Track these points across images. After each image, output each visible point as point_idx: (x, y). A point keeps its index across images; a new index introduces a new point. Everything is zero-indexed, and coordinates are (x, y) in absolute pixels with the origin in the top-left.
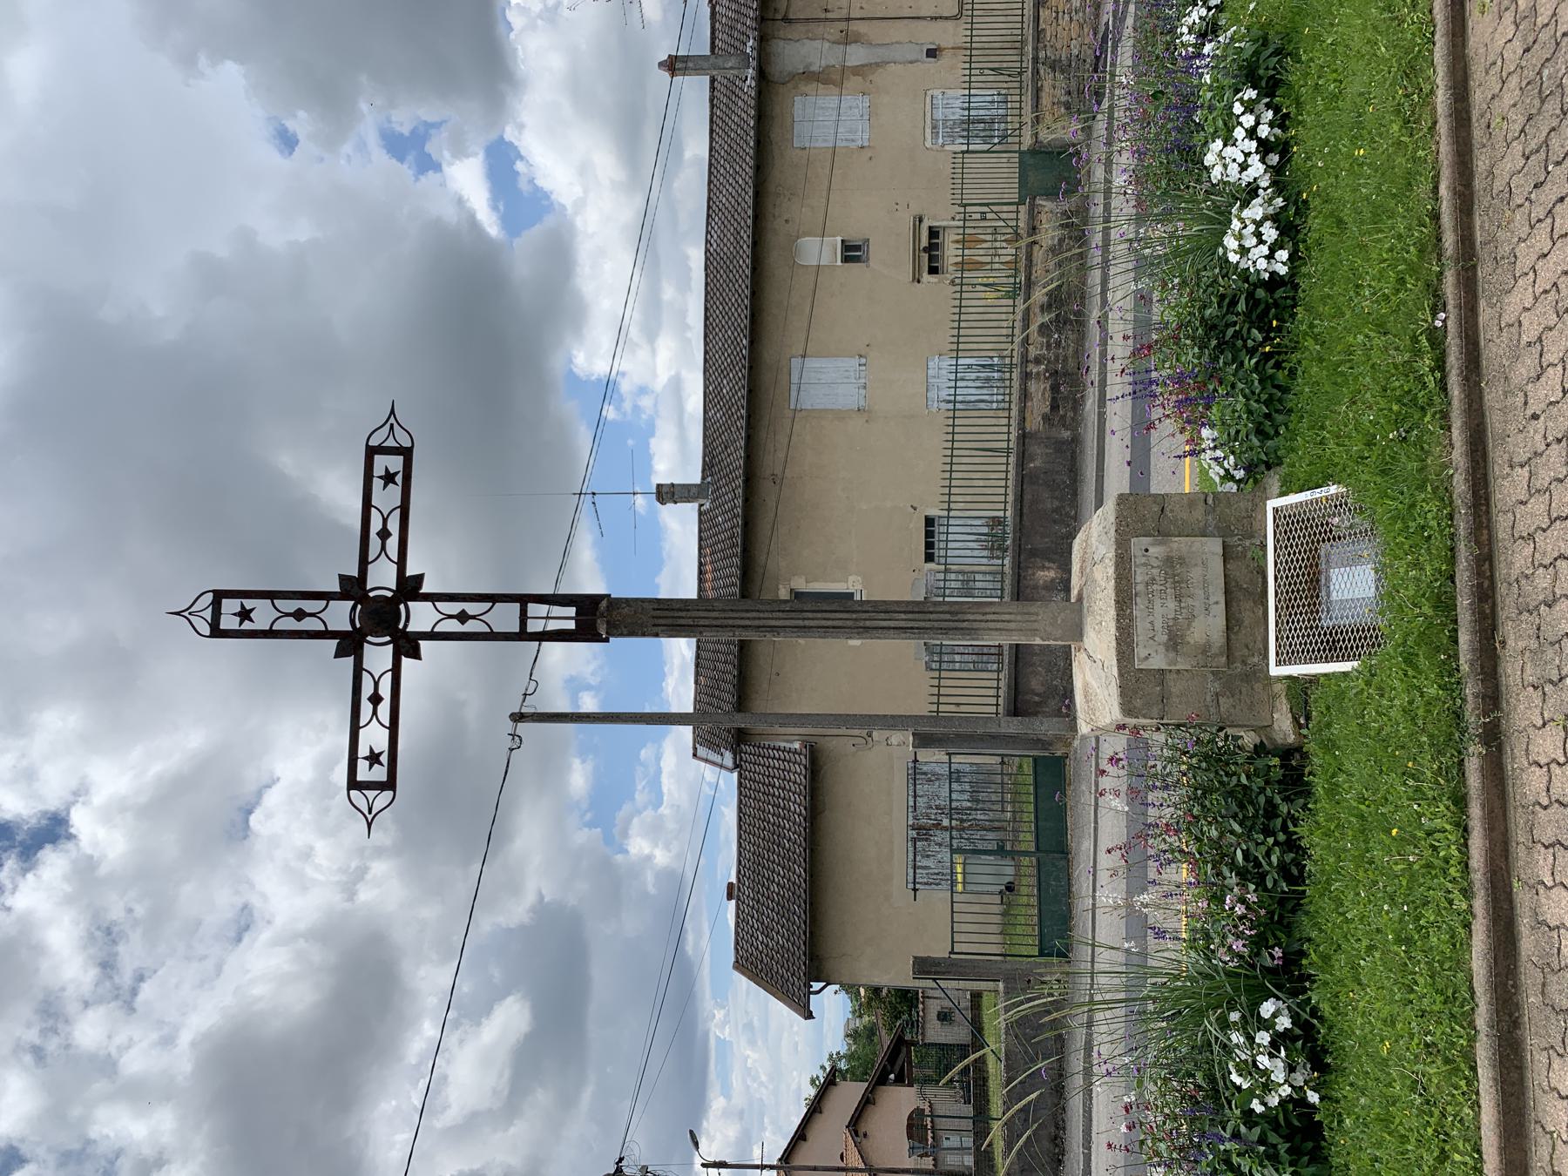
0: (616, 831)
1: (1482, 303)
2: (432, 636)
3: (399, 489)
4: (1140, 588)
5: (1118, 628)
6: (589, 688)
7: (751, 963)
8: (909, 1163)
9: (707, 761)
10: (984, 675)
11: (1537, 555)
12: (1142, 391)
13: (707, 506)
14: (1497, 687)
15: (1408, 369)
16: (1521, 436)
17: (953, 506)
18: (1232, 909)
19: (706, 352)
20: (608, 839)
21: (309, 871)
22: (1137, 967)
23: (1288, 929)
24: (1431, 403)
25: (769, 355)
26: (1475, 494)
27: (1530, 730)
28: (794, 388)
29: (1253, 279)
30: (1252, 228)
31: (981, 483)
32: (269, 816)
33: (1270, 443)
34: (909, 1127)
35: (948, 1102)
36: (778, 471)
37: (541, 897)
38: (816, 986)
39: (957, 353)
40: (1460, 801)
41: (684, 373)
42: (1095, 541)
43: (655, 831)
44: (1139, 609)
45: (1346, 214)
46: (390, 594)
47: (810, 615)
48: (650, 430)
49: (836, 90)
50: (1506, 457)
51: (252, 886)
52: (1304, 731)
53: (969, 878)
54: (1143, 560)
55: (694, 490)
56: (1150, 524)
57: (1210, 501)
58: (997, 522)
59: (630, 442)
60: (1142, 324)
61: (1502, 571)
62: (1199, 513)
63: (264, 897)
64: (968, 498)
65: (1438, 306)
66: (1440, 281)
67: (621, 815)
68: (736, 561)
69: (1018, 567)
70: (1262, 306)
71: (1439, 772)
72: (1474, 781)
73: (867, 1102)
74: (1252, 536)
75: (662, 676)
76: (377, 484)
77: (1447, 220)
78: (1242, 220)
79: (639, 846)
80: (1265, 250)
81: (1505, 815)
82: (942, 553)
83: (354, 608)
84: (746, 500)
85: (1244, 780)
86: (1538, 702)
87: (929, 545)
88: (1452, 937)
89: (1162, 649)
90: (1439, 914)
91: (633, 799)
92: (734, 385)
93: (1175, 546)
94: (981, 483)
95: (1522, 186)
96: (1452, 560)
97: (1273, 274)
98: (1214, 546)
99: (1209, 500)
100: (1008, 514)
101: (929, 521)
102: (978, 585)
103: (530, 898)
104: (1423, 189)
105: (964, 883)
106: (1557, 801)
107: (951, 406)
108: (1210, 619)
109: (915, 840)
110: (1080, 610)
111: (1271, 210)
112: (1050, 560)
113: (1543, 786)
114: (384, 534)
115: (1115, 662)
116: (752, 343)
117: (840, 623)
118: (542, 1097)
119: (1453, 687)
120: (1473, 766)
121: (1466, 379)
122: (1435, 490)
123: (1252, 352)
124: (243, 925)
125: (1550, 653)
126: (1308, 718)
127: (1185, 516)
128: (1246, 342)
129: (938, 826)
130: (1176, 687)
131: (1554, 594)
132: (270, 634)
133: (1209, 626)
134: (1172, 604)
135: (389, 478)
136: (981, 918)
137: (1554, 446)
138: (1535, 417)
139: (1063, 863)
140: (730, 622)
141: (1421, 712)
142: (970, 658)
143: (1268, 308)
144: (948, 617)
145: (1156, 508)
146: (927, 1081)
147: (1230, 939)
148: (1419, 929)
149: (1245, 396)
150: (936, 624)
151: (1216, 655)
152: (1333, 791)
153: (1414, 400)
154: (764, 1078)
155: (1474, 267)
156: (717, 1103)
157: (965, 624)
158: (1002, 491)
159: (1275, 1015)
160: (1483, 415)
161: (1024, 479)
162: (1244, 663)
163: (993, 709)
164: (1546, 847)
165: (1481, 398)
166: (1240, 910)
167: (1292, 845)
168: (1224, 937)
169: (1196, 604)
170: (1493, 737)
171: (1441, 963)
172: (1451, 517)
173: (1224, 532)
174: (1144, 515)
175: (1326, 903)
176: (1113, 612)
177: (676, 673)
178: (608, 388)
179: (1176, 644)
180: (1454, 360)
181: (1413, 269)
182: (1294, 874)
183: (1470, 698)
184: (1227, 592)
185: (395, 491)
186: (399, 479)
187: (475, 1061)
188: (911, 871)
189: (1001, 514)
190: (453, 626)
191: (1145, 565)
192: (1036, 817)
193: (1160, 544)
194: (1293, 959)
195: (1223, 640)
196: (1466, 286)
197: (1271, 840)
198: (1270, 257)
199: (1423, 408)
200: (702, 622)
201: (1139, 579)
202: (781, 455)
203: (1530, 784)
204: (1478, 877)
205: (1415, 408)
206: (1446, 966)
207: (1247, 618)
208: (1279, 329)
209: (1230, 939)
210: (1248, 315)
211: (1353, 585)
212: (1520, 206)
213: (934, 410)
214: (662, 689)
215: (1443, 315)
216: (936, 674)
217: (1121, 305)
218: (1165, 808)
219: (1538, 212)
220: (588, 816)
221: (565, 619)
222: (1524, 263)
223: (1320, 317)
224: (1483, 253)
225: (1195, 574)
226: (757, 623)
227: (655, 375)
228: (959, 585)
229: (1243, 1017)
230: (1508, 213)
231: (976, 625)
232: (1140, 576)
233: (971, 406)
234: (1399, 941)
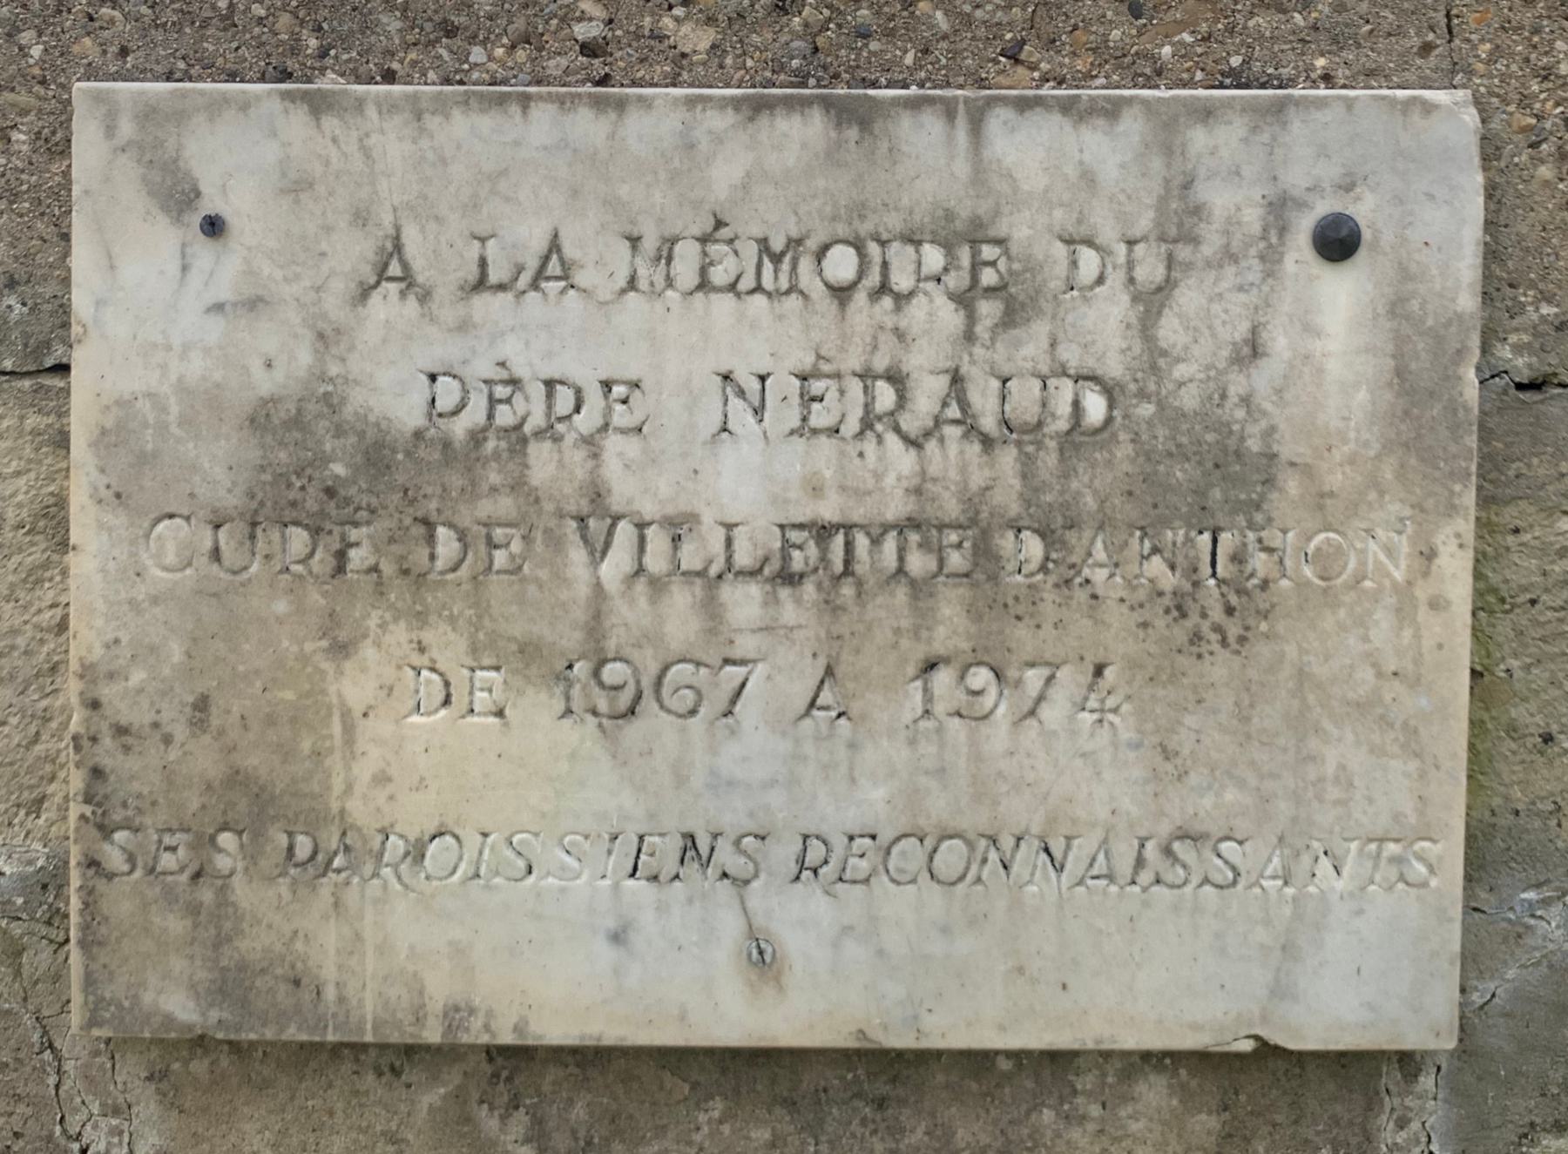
49: (613, 116)
54: (1232, 202)
89: (276, 360)
108: (588, 884)
134: (750, 484)
151: (216, 923)
169: (755, 745)
191: (1180, 223)
193: (1411, 389)
225: (1070, 751)
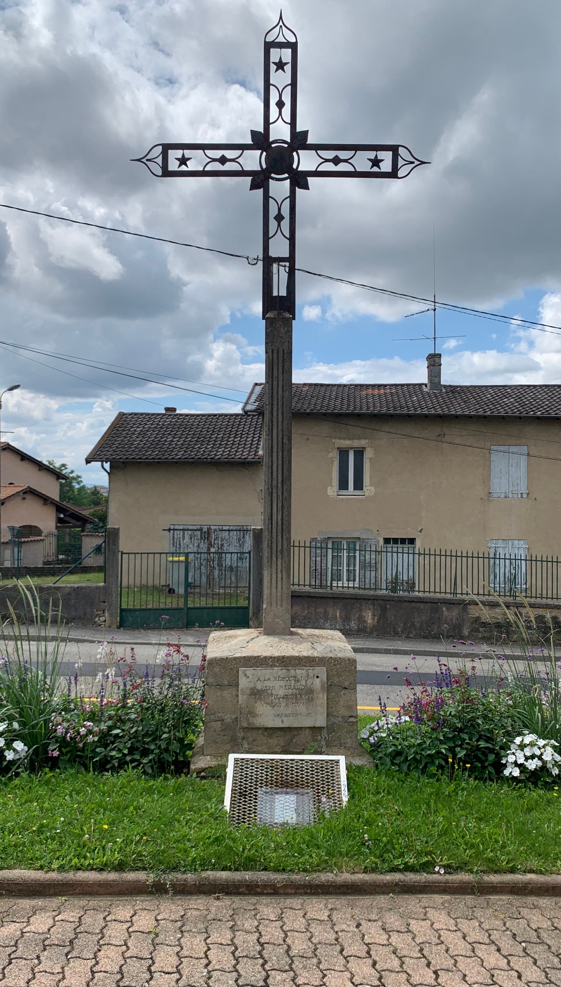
0: (229, 334)
1: (447, 897)
2: (266, 197)
3: (368, 170)
4: (292, 672)
5: (266, 657)
6: (324, 312)
7: (123, 423)
8: (4, 526)
9: (252, 393)
10: (307, 577)
11: (267, 922)
12: (443, 679)
13: (425, 389)
14: (190, 893)
15: (409, 847)
16: (349, 916)
17: (550, 564)
18: (84, 726)
19: (535, 386)
20: (224, 329)
21: (204, 127)
22: (57, 668)
23: (72, 761)
24: (383, 861)
25: (529, 430)
26: (318, 886)
27: (157, 912)
28: (506, 448)
29: (502, 753)
30: (538, 753)
31: (438, 576)
32: (240, 98)
33: (388, 760)
34: (30, 527)
35: (37, 553)
36: (447, 438)
37: (185, 285)
38: (107, 466)
39: (530, 560)
40: (120, 867)
41: (542, 373)
42: (332, 642)
43: (227, 360)
44: (278, 671)
45: (534, 814)
46: (295, 166)
47: (280, 456)
48: (501, 349)
50: (339, 907)
51: (194, 87)
52: (195, 775)
53: (176, 565)
54: (311, 675)
55: (436, 380)
56: (336, 680)
57: (352, 719)
58: (411, 586)
59: (494, 336)
60: (486, 682)
61: (265, 900)
62: (343, 712)
63: (186, 96)
64: (427, 567)
65: (449, 869)
66: (467, 871)
67: (239, 337)
68: (384, 410)
69: (374, 599)
70: (483, 758)
71: (140, 854)
72: (131, 876)
73: (45, 500)
74: (328, 745)
75: (327, 362)
76: (372, 155)
77: (509, 877)
78: (544, 747)
79: (219, 349)
80: (521, 761)
81: (108, 894)
82: (406, 550)
83: (285, 142)
84: (426, 416)
85: (165, 736)
86: (173, 917)
87: (395, 541)
88: (37, 858)
90: (52, 851)
91: (250, 344)
92: (509, 406)
93: (321, 696)
94: (438, 576)
95: (516, 926)
96: (276, 870)
97: (505, 766)
98: (321, 721)
99: (353, 721)
100: (417, 593)
101: (412, 541)
102: (368, 573)
103: (186, 277)
104: (535, 863)
105: (173, 562)
106: (107, 925)
107: (492, 556)
109: (201, 530)
110: (285, 634)
111: (549, 766)
112: (379, 620)
113: (119, 918)
114: (336, 161)
115: (244, 655)
116: (538, 418)
117: (275, 476)
118: (58, 289)
119: (192, 867)
120: (141, 876)
121: (397, 884)
122: (326, 862)
123: (452, 750)
124: (167, 81)
125: (201, 926)
126: (204, 778)
127: (342, 703)
128: (461, 748)
129: (210, 545)
130: (227, 694)
131: (238, 931)
132: (294, 84)
133: (267, 716)
134: (281, 693)
135: (376, 162)
136: (144, 573)
137: (334, 936)
138: (358, 925)
139: (181, 625)
140: (275, 403)
141: (181, 846)
142: (318, 567)
143: (482, 762)
144: (280, 548)
145: (346, 684)
146: (59, 538)
147: (65, 725)
148: (47, 839)
149: (419, 745)
150: (274, 540)
152: (150, 791)
153: (388, 851)
154: (70, 434)
155: (473, 893)
156: (54, 403)
157: (274, 559)
158: (422, 589)
159: (14, 750)
160: (371, 894)
161: (435, 604)
162: (243, 738)
163: (296, 581)
164: (80, 918)
165: (383, 893)
166: (83, 731)
167: (122, 764)
168: (68, 721)
169: (282, 708)
170: (158, 890)
171: (21, 851)
172: (305, 870)
173: (331, 728)
174: (341, 677)
175: (78, 786)
176: (277, 654)
177: (330, 372)
178: (532, 322)
179: (255, 695)
180: (411, 877)
181: (478, 854)
182: (103, 766)
183: (185, 876)
184: (290, 729)
185: (366, 167)
186: (375, 169)
187: (77, 245)
188: (181, 527)
189: (417, 589)
190: (273, 211)
191: (308, 676)
192: (209, 608)
193: (322, 686)
194: (54, 763)
195: (258, 725)
196: (461, 888)
197: (126, 752)
198: (516, 764)
199: (382, 856)
200: (275, 383)
201: (298, 671)
202: (458, 440)
203: (122, 910)
204: (71, 876)
205: (384, 853)
206: (19, 854)
207: (273, 741)
208: (465, 769)
209: (65, 725)
210: (478, 748)
211: (283, 809)
212: (505, 924)
213: (489, 545)
214: (318, 362)
215: (442, 871)
216: (308, 544)
217: (485, 664)
218: (158, 688)
219: (495, 935)
220: (239, 315)
221: (280, 289)
222: (464, 925)
223: (469, 795)
224: (482, 900)
225: (302, 708)
226: (275, 420)
227: (542, 352)
228: (368, 560)
229: (15, 730)
230: (502, 916)
231: (274, 566)
232: (300, 672)
233: (491, 570)
234: (42, 826)
